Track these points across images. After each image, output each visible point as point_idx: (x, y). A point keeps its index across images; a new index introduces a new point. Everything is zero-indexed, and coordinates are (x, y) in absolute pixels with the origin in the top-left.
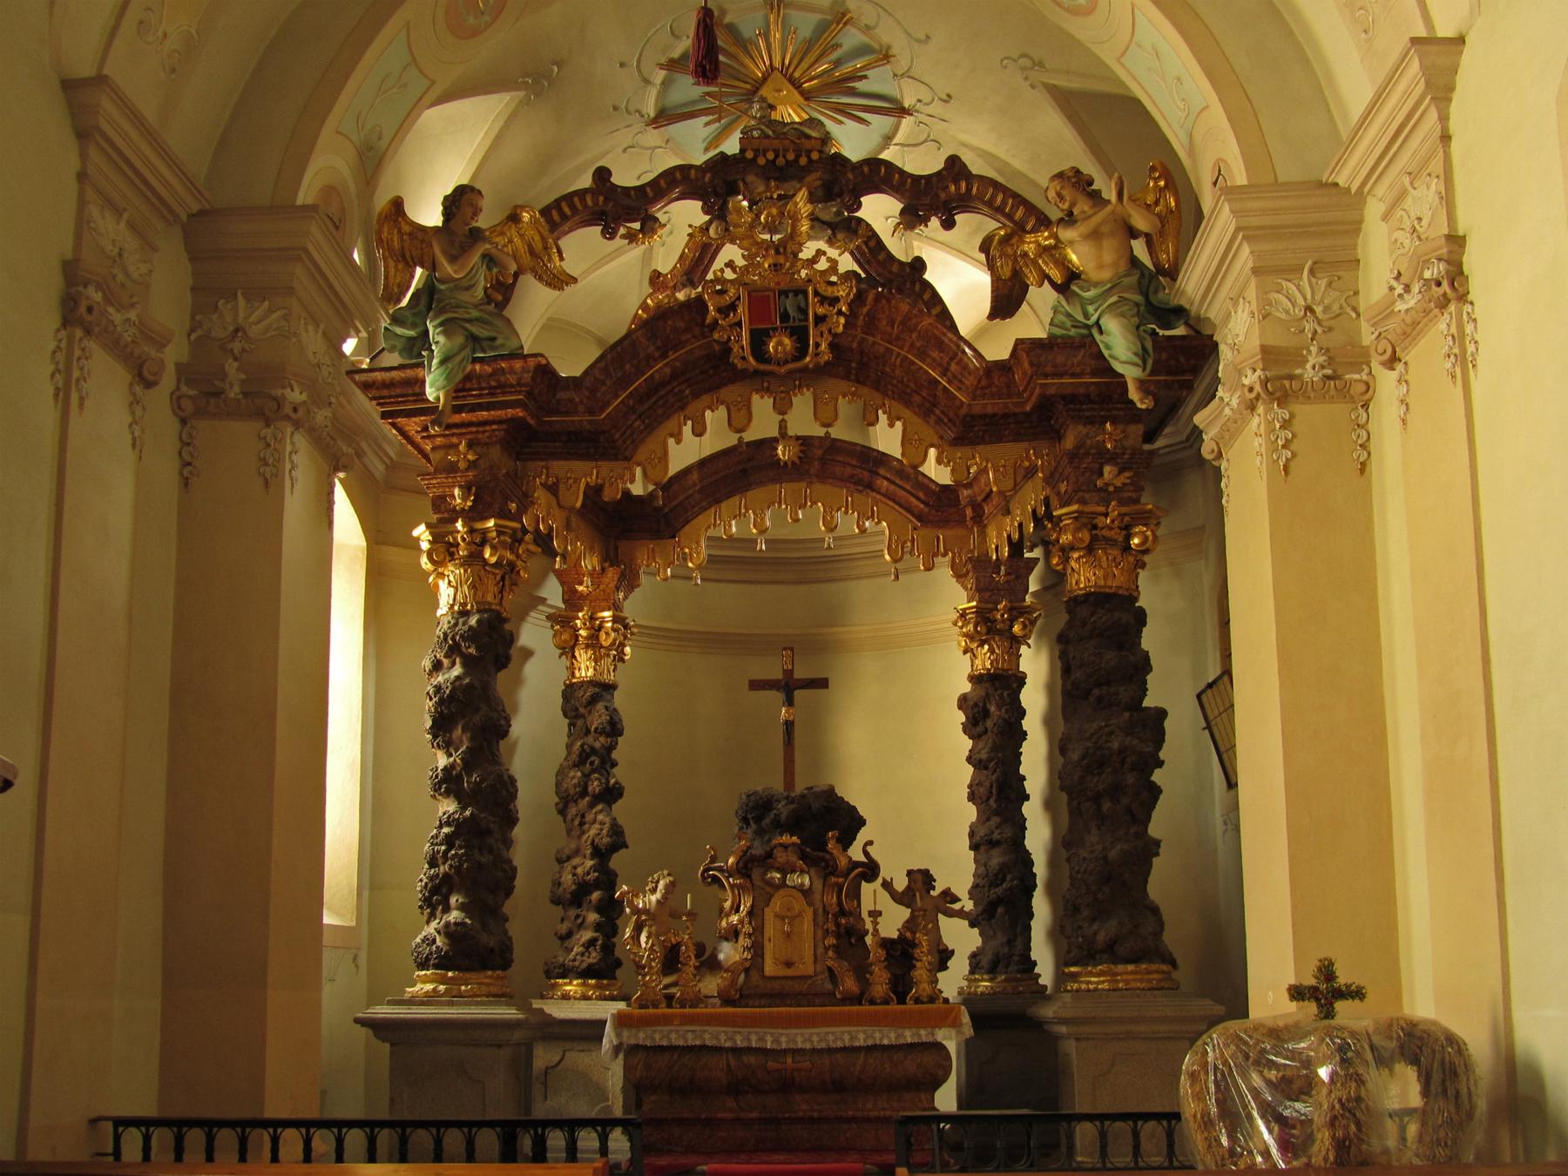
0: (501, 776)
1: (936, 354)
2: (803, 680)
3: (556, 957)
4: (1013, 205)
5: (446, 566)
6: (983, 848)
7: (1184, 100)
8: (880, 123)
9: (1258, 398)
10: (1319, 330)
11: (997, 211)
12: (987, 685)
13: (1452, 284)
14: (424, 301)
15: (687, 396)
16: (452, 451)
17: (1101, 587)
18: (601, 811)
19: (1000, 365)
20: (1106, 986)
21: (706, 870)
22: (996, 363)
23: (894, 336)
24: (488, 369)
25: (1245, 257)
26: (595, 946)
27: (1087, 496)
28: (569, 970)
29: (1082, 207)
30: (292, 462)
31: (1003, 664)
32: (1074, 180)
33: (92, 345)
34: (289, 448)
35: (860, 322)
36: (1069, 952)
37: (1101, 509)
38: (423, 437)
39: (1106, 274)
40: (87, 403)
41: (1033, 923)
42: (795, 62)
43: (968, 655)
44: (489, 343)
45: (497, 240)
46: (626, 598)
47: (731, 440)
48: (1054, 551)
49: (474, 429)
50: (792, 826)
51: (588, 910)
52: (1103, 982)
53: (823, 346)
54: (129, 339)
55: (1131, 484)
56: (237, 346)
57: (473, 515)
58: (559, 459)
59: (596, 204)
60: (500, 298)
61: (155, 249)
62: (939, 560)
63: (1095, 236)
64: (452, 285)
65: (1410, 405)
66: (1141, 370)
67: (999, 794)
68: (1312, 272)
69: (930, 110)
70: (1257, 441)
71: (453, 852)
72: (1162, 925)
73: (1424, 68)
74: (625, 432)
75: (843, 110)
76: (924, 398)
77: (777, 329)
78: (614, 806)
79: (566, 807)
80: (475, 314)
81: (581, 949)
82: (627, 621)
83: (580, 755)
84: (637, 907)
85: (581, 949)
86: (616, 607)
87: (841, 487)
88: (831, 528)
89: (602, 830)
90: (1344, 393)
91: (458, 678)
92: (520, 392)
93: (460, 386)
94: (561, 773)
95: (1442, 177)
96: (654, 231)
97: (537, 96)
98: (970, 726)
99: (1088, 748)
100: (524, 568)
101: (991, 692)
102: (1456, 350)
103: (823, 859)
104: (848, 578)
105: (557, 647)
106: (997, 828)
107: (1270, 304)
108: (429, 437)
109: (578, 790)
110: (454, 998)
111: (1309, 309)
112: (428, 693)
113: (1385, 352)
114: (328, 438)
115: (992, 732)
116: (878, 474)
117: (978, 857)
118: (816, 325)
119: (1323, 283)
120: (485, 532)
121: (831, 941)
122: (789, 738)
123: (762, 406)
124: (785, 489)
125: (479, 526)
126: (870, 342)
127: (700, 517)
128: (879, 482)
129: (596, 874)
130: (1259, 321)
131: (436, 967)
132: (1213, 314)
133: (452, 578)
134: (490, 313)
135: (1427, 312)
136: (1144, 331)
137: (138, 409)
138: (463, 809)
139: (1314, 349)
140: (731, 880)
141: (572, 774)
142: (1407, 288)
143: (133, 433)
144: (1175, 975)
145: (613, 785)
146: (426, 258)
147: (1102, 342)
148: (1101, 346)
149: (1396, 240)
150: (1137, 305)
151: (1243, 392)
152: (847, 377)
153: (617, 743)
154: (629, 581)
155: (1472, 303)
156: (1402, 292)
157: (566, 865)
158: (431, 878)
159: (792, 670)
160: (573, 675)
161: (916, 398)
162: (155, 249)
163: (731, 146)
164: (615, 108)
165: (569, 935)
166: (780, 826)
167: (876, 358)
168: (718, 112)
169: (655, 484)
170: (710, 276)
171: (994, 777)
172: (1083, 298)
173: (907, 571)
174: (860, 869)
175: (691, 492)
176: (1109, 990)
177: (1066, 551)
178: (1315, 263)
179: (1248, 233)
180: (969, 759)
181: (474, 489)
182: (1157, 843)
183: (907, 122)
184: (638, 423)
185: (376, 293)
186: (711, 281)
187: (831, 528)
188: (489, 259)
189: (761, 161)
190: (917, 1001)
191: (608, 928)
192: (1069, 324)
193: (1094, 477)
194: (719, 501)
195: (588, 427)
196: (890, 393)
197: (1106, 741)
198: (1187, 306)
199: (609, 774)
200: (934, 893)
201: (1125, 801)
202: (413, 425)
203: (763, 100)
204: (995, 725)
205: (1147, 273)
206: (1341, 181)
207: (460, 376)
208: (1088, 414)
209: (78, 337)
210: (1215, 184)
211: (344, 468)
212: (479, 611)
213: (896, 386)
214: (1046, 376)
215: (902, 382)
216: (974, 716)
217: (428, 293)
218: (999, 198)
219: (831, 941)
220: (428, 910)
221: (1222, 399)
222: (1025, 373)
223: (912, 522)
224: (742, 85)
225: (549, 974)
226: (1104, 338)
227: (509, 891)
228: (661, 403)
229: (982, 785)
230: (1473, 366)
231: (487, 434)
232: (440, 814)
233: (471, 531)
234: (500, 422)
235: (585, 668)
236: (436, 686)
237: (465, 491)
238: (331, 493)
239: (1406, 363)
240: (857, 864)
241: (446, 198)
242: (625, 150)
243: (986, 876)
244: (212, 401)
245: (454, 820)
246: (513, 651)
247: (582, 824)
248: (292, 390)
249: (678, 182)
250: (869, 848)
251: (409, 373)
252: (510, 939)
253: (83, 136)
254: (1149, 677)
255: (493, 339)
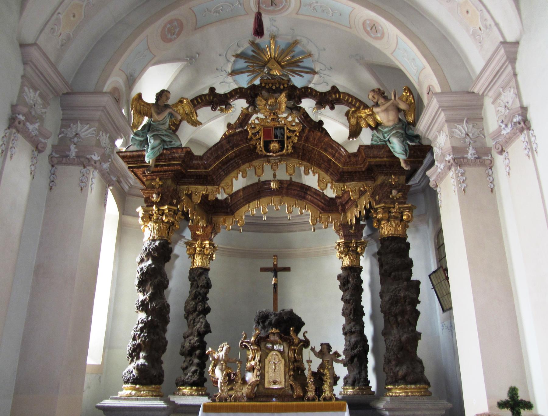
0: (164, 304)
1: (330, 150)
2: (281, 268)
3: (181, 377)
4: (355, 102)
5: (148, 223)
6: (348, 334)
7: (416, 66)
8: (307, 76)
9: (452, 165)
10: (472, 142)
11: (349, 104)
12: (348, 271)
13: (524, 123)
14: (147, 128)
15: (240, 164)
16: (153, 181)
17: (393, 234)
18: (201, 318)
19: (354, 155)
20: (403, 394)
21: (242, 342)
22: (352, 153)
23: (315, 144)
24: (169, 152)
25: (442, 117)
26: (196, 373)
27: (386, 201)
28: (186, 383)
29: (381, 101)
30: (92, 182)
31: (354, 263)
32: (378, 92)
33: (19, 136)
34: (91, 176)
35: (303, 139)
36: (387, 379)
37: (392, 206)
38: (143, 176)
39: (391, 124)
40: (14, 156)
41: (368, 365)
42: (279, 56)
43: (341, 260)
44: (169, 143)
45: (174, 109)
46: (214, 236)
47: (256, 180)
48: (374, 221)
49: (162, 173)
50: (277, 325)
51: (194, 358)
52: (402, 393)
53: (290, 147)
54: (34, 135)
55: (402, 197)
56: (76, 140)
57: (159, 204)
58: (192, 185)
59: (210, 99)
60: (174, 128)
61: (48, 104)
62: (329, 224)
63: (386, 110)
64: (157, 123)
65: (511, 167)
66: (405, 156)
67: (354, 313)
68: (467, 122)
69: (325, 72)
70: (453, 180)
71: (143, 335)
72: (423, 368)
73: (506, 52)
74: (217, 176)
75: (295, 72)
76: (326, 166)
77: (273, 141)
78: (207, 316)
79: (188, 316)
80: (165, 133)
81: (191, 374)
82: (215, 245)
83: (195, 296)
84: (214, 358)
85: (191, 374)
86: (211, 240)
87: (294, 198)
88: (290, 212)
89: (201, 325)
90: (483, 164)
91: (150, 265)
92: (180, 160)
93: (158, 158)
94: (187, 303)
95: (515, 88)
96: (229, 108)
97: (190, 64)
98: (342, 286)
99: (391, 296)
100: (177, 224)
101: (350, 274)
102: (529, 147)
103: (289, 339)
104: (296, 231)
105: (188, 254)
106: (353, 326)
107: (453, 133)
108: (145, 176)
109: (193, 309)
110: (139, 397)
111: (467, 135)
112: (138, 271)
113: (499, 148)
114: (107, 174)
115: (351, 289)
116: (307, 194)
117: (346, 338)
118: (287, 139)
119: (471, 126)
120: (163, 210)
121: (292, 373)
122: (275, 290)
123: (267, 167)
124: (273, 199)
125: (162, 208)
126: (307, 146)
127: (243, 208)
128: (307, 196)
129: (198, 343)
130: (450, 138)
131: (132, 383)
132: (431, 136)
133: (150, 227)
134: (170, 133)
135: (515, 134)
136: (405, 143)
137: (35, 161)
138: (148, 317)
139: (471, 148)
140: (252, 347)
141: (191, 303)
142: (506, 126)
143: (31, 169)
144: (430, 389)
145: (207, 307)
146: (148, 114)
147: (391, 146)
148: (390, 148)
149: (498, 110)
150: (402, 134)
151: (446, 162)
152: (298, 158)
153: (209, 291)
154: (215, 231)
155: (533, 130)
156: (504, 127)
157: (187, 339)
158: (133, 345)
159: (277, 264)
160: (193, 265)
161: (323, 166)
162: (48, 104)
163: (257, 82)
164: (217, 69)
165: (186, 368)
166: (271, 325)
167: (309, 151)
168: (252, 71)
169: (228, 194)
170: (250, 122)
171: (352, 306)
172: (383, 132)
173: (318, 229)
174: (302, 343)
175: (240, 199)
176: (405, 396)
177: (379, 221)
178: (468, 119)
179: (443, 108)
180: (342, 299)
181: (161, 195)
182: (420, 334)
183: (316, 77)
184: (222, 173)
185: (130, 125)
186: (250, 124)
187: (290, 212)
188: (171, 115)
189: (267, 87)
190: (325, 399)
191: (202, 366)
192: (378, 140)
193: (389, 194)
194: (249, 202)
195: (204, 173)
196: (313, 164)
197: (398, 293)
198: (420, 135)
199: (205, 303)
200: (331, 353)
201: (407, 317)
202: (139, 172)
203: (268, 67)
204: (352, 286)
205: (404, 124)
206: (476, 91)
207: (158, 154)
208: (385, 172)
209: (13, 132)
210: (428, 93)
211: (112, 185)
212: (159, 240)
213: (316, 161)
214: (371, 158)
215: (318, 160)
216: (344, 283)
217: (148, 127)
218: (350, 100)
219: (292, 373)
220: (131, 359)
221: (437, 166)
222: (363, 157)
223: (320, 211)
224: (261, 63)
225: (177, 384)
226: (391, 145)
227: (164, 351)
228: (231, 166)
229: (347, 310)
230: (536, 152)
231: (167, 175)
232: (139, 319)
233: (159, 210)
234: (172, 171)
235: (198, 262)
236: (141, 268)
237: (157, 195)
238: (106, 194)
239: (507, 152)
240: (301, 341)
241: (157, 94)
242: (220, 83)
243: (350, 346)
244: (64, 159)
245: (144, 321)
246: (172, 255)
247: (194, 323)
248: (95, 156)
249: (238, 93)
250: (306, 334)
251: (140, 153)
252: (163, 371)
253: (25, 63)
254: (412, 268)
255: (171, 142)
